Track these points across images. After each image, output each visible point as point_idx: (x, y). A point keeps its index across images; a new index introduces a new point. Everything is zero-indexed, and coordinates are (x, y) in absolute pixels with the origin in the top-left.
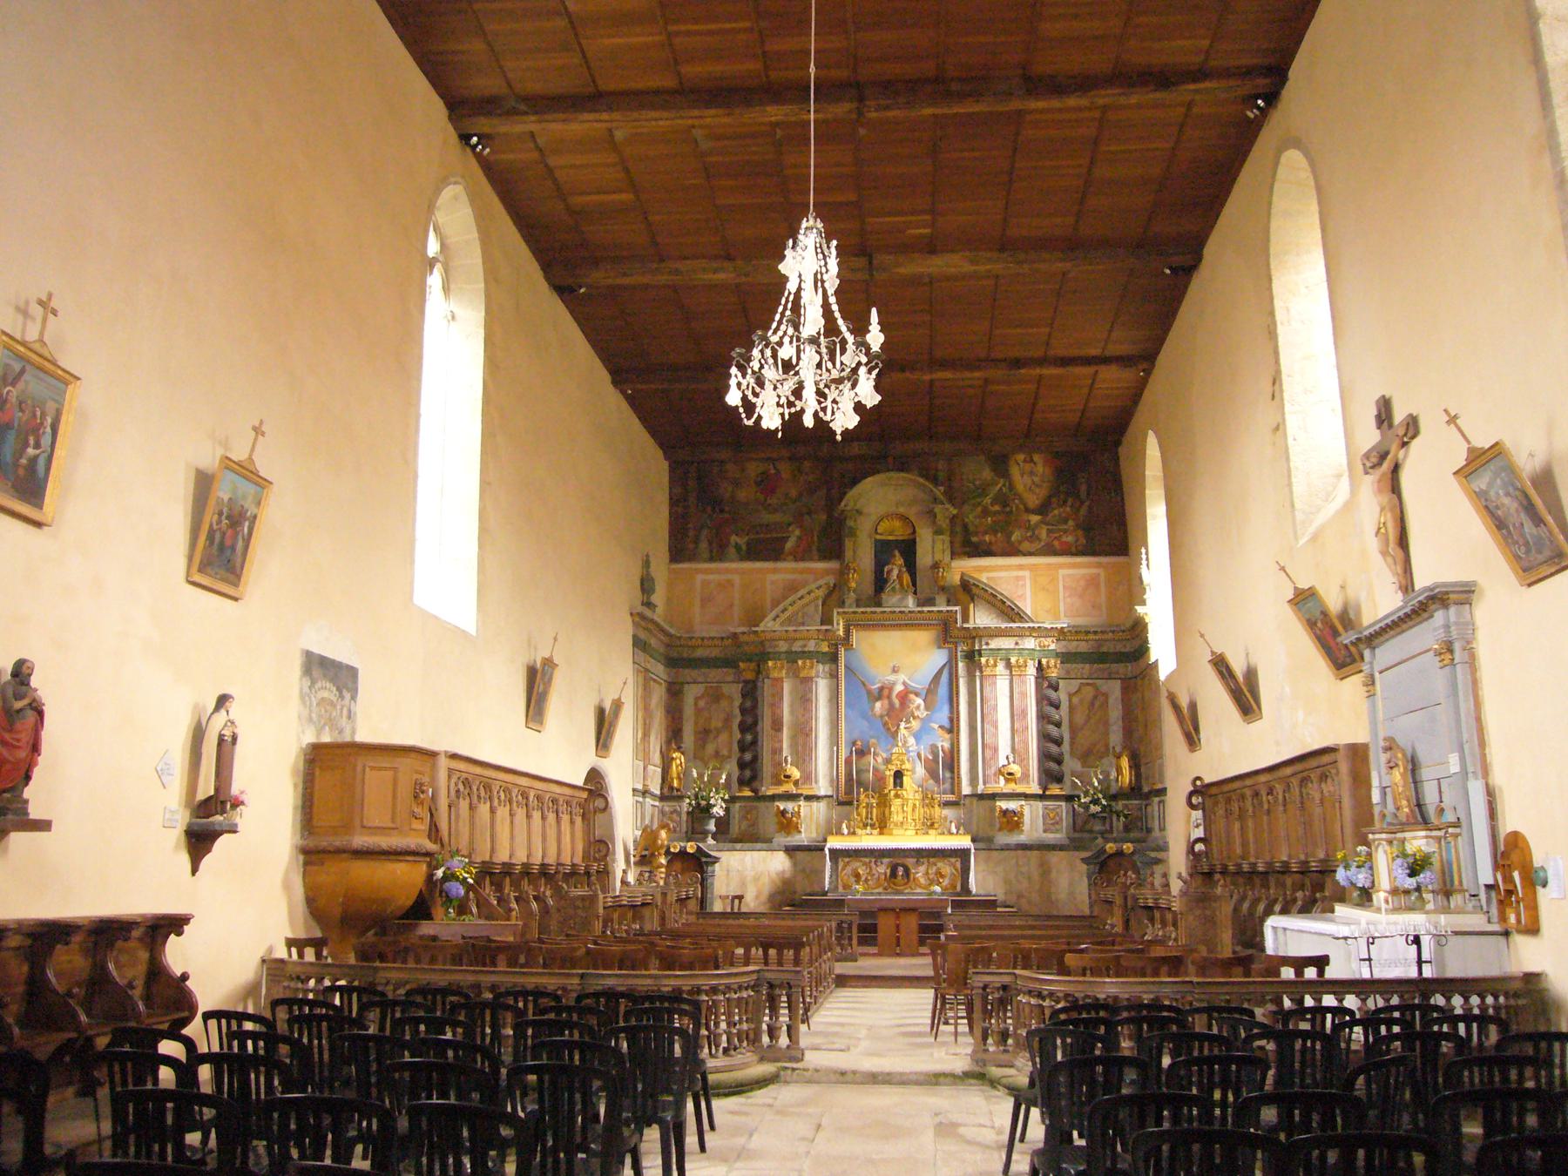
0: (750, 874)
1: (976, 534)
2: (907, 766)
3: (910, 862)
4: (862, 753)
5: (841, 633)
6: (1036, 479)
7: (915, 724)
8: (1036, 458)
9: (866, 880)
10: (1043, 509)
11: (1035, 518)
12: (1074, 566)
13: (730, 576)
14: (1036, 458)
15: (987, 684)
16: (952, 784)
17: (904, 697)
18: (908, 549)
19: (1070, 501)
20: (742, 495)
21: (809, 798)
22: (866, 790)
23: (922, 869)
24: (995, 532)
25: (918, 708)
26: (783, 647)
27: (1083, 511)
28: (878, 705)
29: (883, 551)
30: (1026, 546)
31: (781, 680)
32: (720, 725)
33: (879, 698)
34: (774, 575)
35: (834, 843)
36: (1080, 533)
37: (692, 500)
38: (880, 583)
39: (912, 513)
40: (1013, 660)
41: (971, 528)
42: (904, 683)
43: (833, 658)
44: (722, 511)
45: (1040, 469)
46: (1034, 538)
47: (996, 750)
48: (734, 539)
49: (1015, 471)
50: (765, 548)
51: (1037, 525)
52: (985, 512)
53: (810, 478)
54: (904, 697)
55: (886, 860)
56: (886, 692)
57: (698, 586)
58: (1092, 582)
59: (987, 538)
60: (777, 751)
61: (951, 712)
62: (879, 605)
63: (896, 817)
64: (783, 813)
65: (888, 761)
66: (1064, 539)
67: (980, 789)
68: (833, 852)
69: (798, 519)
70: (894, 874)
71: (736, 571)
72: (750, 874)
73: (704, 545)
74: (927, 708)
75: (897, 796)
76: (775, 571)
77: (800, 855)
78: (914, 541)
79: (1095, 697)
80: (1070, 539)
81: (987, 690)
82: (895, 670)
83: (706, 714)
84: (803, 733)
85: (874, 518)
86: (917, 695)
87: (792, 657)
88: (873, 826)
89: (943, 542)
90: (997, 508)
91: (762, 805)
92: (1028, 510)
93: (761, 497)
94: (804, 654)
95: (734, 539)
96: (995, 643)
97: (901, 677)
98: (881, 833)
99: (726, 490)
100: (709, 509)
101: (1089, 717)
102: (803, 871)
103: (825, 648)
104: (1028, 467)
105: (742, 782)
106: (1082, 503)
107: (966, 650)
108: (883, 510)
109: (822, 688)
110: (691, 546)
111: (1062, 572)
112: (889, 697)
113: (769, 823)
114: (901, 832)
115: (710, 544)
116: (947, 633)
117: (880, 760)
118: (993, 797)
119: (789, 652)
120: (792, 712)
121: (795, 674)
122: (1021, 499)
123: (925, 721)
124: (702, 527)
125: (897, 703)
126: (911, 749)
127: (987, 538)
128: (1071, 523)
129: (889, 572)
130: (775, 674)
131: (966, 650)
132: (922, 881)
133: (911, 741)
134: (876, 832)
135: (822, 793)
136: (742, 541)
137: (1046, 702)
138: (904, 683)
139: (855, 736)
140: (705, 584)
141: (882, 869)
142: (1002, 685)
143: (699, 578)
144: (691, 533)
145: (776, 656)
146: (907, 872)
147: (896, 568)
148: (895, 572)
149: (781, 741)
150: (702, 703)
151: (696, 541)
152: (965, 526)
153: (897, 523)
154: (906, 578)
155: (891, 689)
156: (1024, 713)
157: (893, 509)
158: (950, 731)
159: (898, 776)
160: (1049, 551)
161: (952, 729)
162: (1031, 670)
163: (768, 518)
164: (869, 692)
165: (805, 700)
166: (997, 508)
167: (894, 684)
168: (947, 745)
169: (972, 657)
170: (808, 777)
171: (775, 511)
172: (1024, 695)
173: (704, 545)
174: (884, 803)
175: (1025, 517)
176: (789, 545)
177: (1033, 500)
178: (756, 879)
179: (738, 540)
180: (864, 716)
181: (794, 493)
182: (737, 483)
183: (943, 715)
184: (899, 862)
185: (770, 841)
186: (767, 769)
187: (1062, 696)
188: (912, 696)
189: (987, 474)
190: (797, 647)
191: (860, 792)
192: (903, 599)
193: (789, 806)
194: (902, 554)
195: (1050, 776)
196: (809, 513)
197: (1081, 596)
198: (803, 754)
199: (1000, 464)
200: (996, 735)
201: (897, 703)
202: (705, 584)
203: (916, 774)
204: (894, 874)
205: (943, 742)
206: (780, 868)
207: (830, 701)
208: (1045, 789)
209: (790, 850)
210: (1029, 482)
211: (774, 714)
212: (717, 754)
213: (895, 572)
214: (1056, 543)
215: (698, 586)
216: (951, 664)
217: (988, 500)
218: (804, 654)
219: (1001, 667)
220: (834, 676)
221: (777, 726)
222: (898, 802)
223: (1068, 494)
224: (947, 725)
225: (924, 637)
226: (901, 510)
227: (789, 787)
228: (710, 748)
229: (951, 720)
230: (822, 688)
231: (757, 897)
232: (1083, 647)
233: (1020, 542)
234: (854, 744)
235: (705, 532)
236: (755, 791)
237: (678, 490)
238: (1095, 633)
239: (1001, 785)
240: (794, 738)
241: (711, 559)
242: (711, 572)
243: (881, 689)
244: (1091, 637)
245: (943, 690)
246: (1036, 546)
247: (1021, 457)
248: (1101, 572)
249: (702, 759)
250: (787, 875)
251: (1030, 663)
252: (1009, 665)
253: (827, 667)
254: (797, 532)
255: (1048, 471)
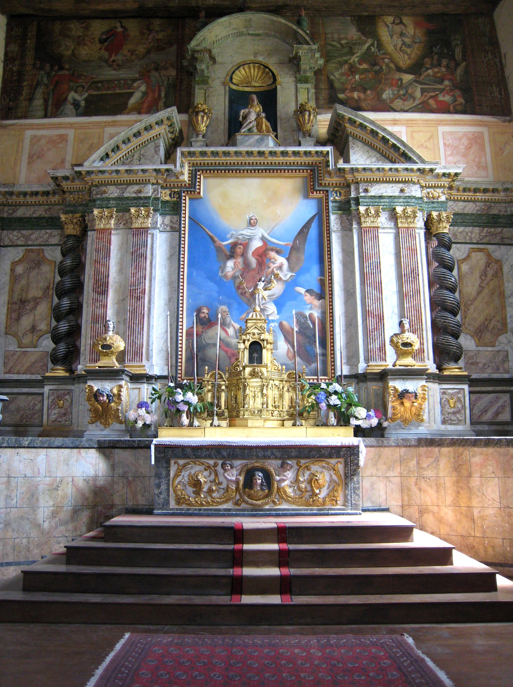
0: (43, 482)
1: (343, 91)
2: (266, 336)
3: (272, 465)
4: (206, 323)
5: (186, 177)
6: (407, 40)
7: (277, 288)
8: (406, 20)
9: (210, 491)
10: (416, 69)
11: (407, 78)
12: (456, 123)
13: (62, 132)
14: (406, 20)
15: (367, 238)
16: (324, 363)
17: (262, 255)
18: (269, 99)
19: (444, 62)
20: (84, 52)
21: (136, 378)
22: (212, 368)
23: (290, 475)
24: (365, 90)
25: (280, 268)
26: (113, 192)
27: (459, 71)
28: (230, 264)
29: (238, 100)
30: (398, 103)
31: (107, 232)
32: (40, 294)
33: (232, 256)
34: (118, 128)
35: (167, 436)
36: (457, 93)
37: (30, 54)
38: (234, 125)
39: (272, 63)
40: (399, 209)
41: (337, 85)
42: (263, 239)
43: (175, 208)
44: (61, 68)
45: (411, 30)
46: (407, 96)
47: (381, 318)
48: (72, 95)
49: (384, 33)
50: (106, 103)
51: (410, 83)
52: (353, 70)
53: (160, 36)
54: (262, 255)
55: (238, 463)
56: (239, 250)
57: (27, 142)
58: (476, 140)
59: (355, 95)
60: (101, 320)
61: (322, 273)
62: (234, 145)
63: (254, 402)
64: (97, 395)
65: (242, 332)
66: (441, 98)
67: (362, 367)
68: (161, 449)
69: (144, 76)
70: (249, 482)
71: (71, 126)
72: (43, 482)
73: (38, 102)
74: (291, 269)
75: (254, 374)
76: (114, 124)
77: (120, 454)
78: (275, 89)
79: (488, 265)
80: (447, 98)
81: (368, 246)
82: (252, 223)
83: (23, 282)
84: (135, 294)
85: (229, 67)
86: (278, 252)
87: (123, 206)
88: (220, 416)
89: (306, 94)
90: (365, 66)
91: (76, 388)
92: (399, 69)
93: (106, 55)
94: (141, 201)
95: (72, 95)
96: (375, 190)
97: (259, 232)
98: (231, 425)
99: (66, 48)
100: (48, 67)
101: (481, 288)
102: (124, 476)
103: (165, 196)
104: (398, 29)
105: (55, 360)
106: (457, 65)
107: (338, 200)
108: (239, 59)
109: (159, 243)
110: (24, 104)
111: (442, 129)
112: (244, 255)
113: (82, 411)
114: (259, 423)
115: (46, 101)
116: (313, 178)
117: (231, 331)
118: (383, 376)
119: (119, 199)
120: (121, 271)
121: (126, 224)
122: (392, 60)
123: (290, 285)
124: (38, 84)
125: (253, 262)
126: (271, 315)
127: (355, 95)
128: (447, 83)
129: (245, 117)
130: (100, 225)
131: (338, 200)
132: (290, 491)
133: (272, 308)
134: (224, 423)
135: (156, 371)
136: (81, 98)
137: (441, 263)
138: (263, 239)
139: (202, 299)
140: (35, 140)
141: (233, 475)
142: (386, 241)
143: (29, 133)
144: (25, 91)
145: (105, 203)
146: (268, 477)
147: (254, 112)
148: (253, 117)
149: (105, 306)
150: (19, 269)
151: (31, 99)
152: (331, 85)
153: (255, 72)
154: (265, 124)
155: (246, 246)
156: (414, 274)
157: (252, 58)
158: (321, 296)
159: (256, 348)
160: (424, 108)
161: (324, 292)
162: (420, 223)
163: (109, 73)
164: (219, 249)
165: (137, 256)
166: (365, 66)
167: (250, 239)
168: (316, 314)
169: (347, 209)
170: (136, 351)
171: (119, 67)
172: (413, 251)
173: (38, 102)
174: (236, 383)
175: (397, 76)
176: (132, 101)
177: (404, 61)
178: (54, 488)
179: (77, 97)
180: (212, 277)
181: (141, 49)
182: (80, 41)
183: (312, 277)
184: (257, 465)
185: (80, 434)
186: (85, 342)
187: (457, 252)
188: (273, 254)
189: (353, 33)
190: (130, 192)
191: (208, 373)
192: (262, 140)
193: (107, 386)
194: (261, 102)
195: (444, 354)
196: (157, 69)
197: (464, 155)
198: (134, 319)
199: (367, 23)
200: (380, 300)
201: (253, 262)
202: (35, 140)
203: (278, 352)
204: (249, 482)
205: (313, 310)
206: (91, 472)
207: (170, 258)
208: (439, 368)
209: (105, 448)
210: (400, 43)
211: (97, 272)
212: (33, 329)
213: (253, 117)
214: (432, 102)
215: (27, 142)
216: (321, 218)
217: (355, 59)
218: (141, 201)
219: (383, 219)
220: (175, 229)
221: (102, 288)
222: (254, 383)
223: (441, 55)
224: (316, 288)
225: (286, 186)
226: (260, 59)
227: (113, 362)
228: (26, 322)
229: (322, 283)
230: (159, 243)
231: (54, 514)
232: (470, 208)
233: (392, 101)
234: (199, 311)
235: (40, 91)
236: (71, 371)
237: (14, 48)
238: (485, 191)
239: (391, 359)
240: (121, 302)
241: (46, 116)
242: (39, 127)
243: (234, 245)
244: (479, 196)
245: (311, 246)
246: (409, 104)
247: (390, 19)
248: (484, 130)
249: (15, 335)
250: (101, 482)
251: (419, 214)
252: (394, 216)
253: (167, 219)
254: (143, 88)
255: (420, 34)
